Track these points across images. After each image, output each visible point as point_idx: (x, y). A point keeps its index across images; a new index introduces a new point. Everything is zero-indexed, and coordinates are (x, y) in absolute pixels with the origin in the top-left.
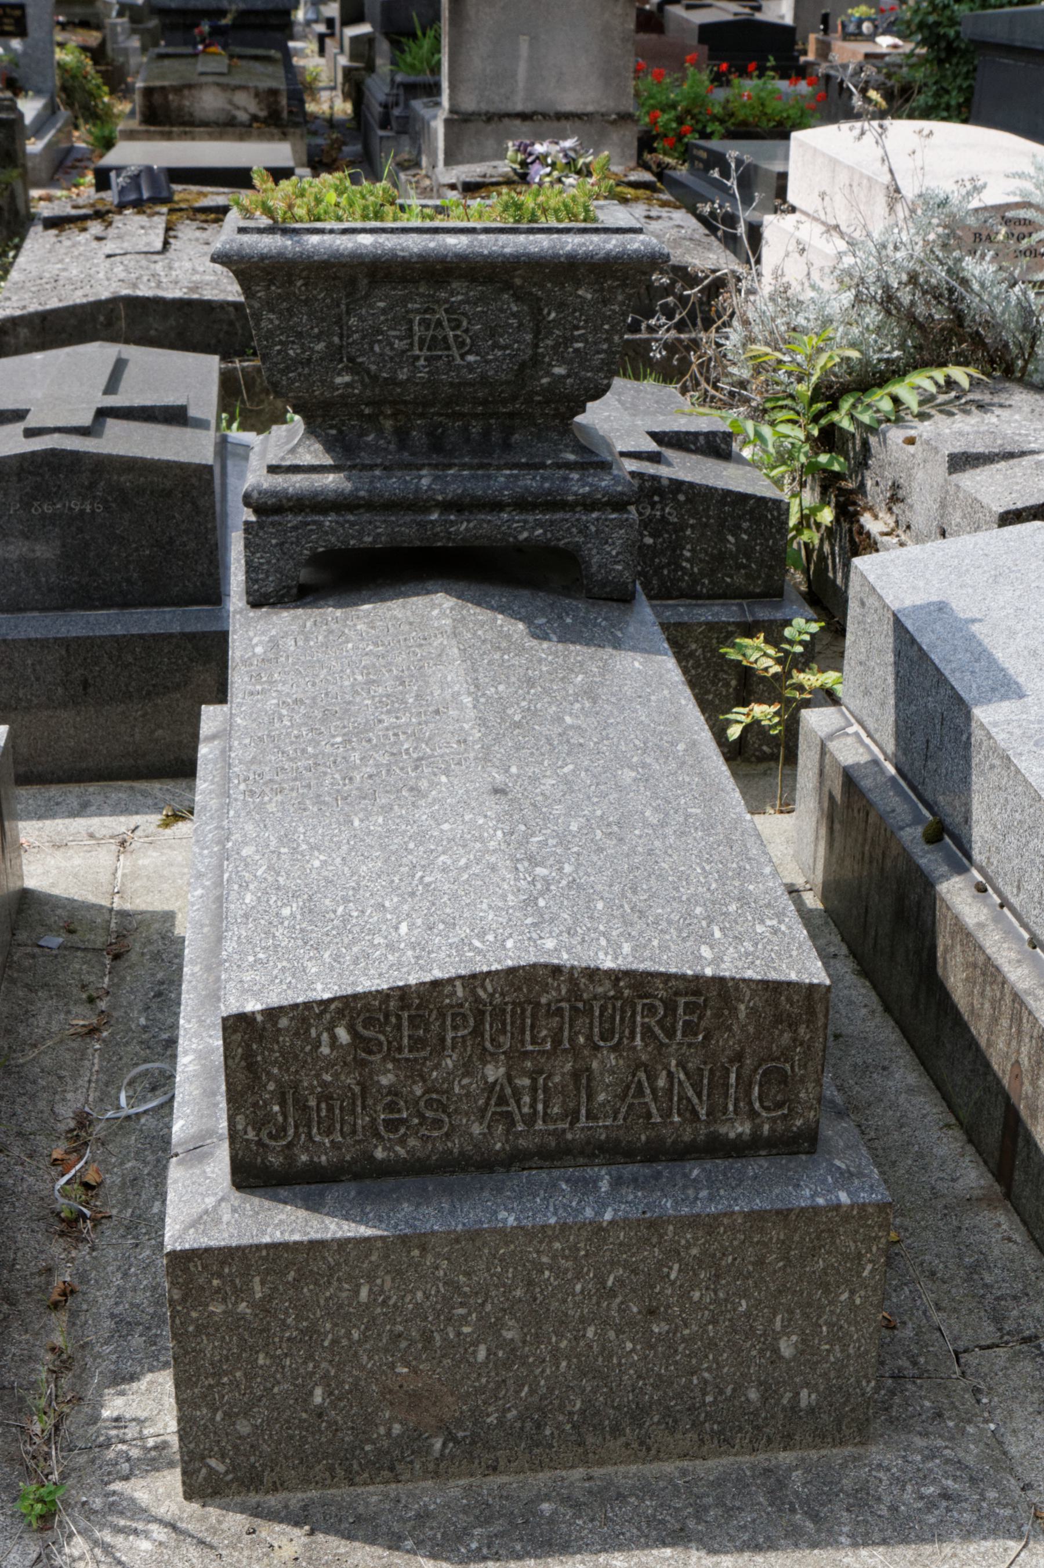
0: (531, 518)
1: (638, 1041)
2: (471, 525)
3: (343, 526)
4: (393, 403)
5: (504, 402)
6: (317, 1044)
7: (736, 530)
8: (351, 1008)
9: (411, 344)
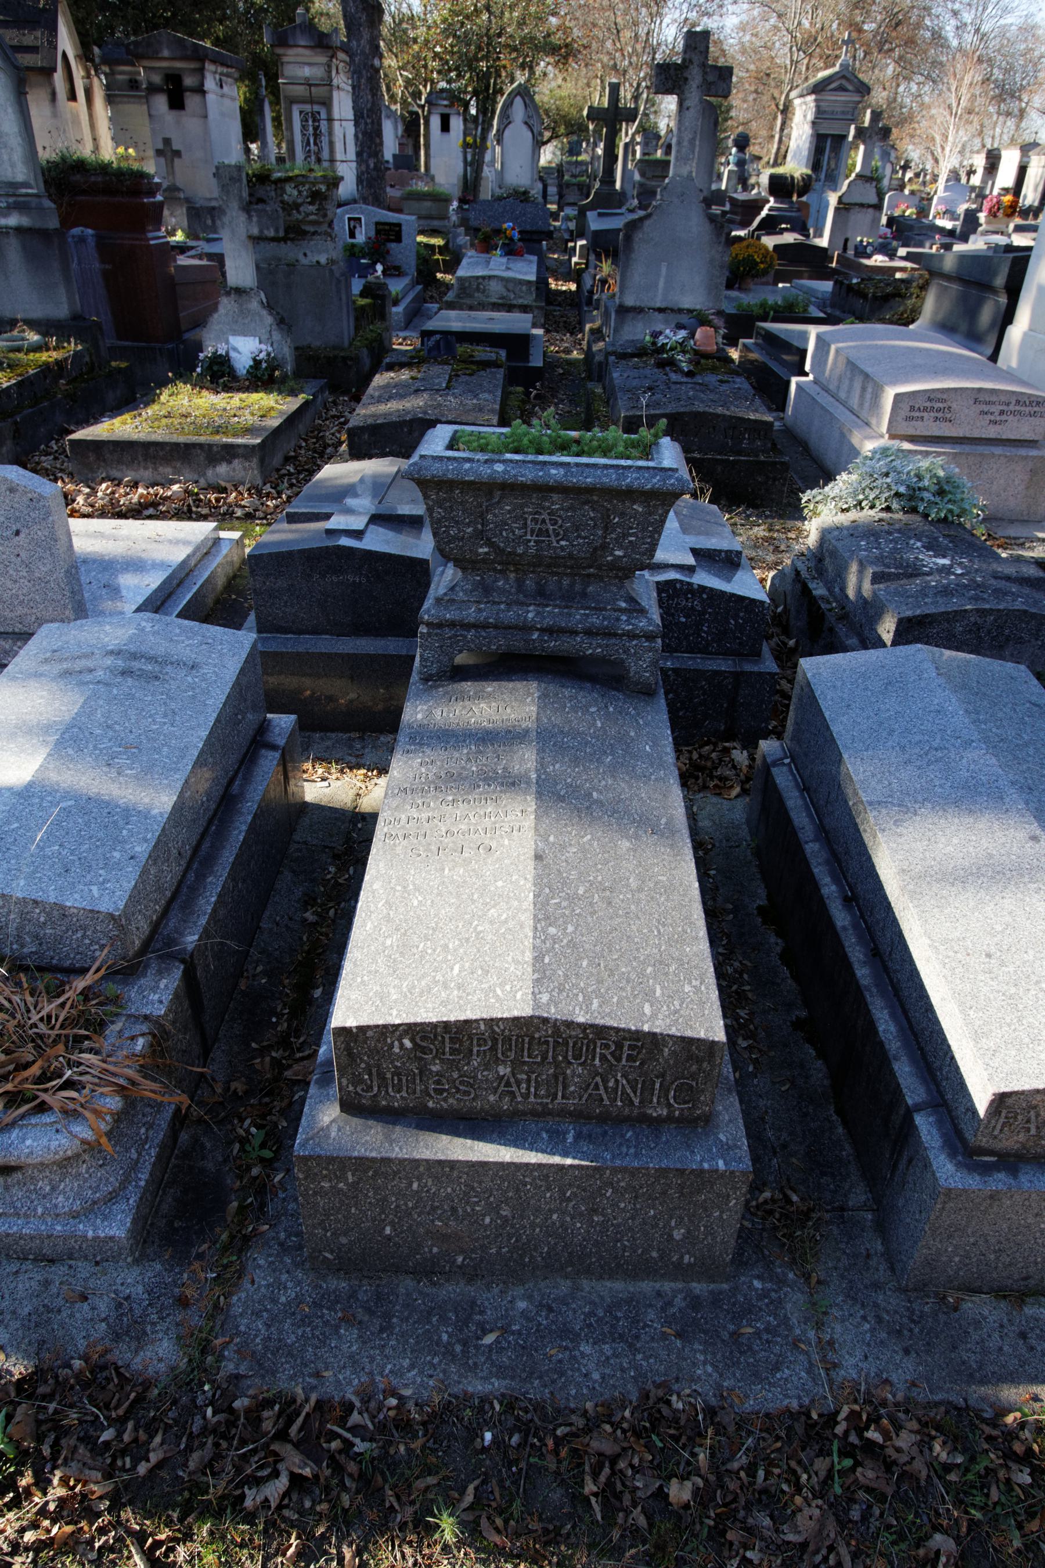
1: (597, 1062)
4: (515, 565)
5: (584, 568)
6: (392, 1046)
7: (736, 617)
8: (412, 1029)
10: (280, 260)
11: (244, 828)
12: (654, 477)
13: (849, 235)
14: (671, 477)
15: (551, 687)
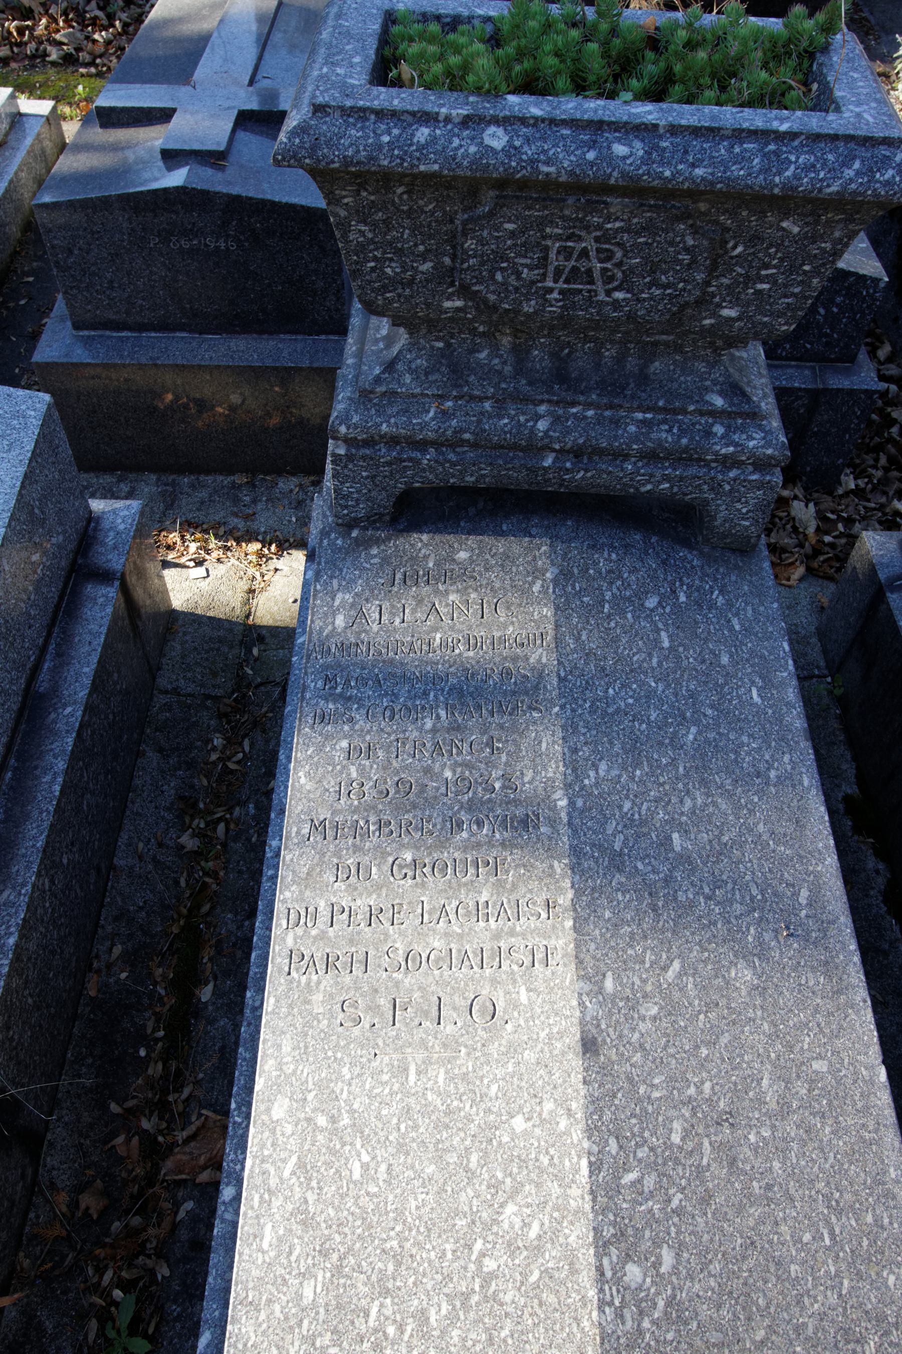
3: (442, 465)
9: (544, 275)
11: (61, 765)
12: (846, 163)
14: (886, 161)
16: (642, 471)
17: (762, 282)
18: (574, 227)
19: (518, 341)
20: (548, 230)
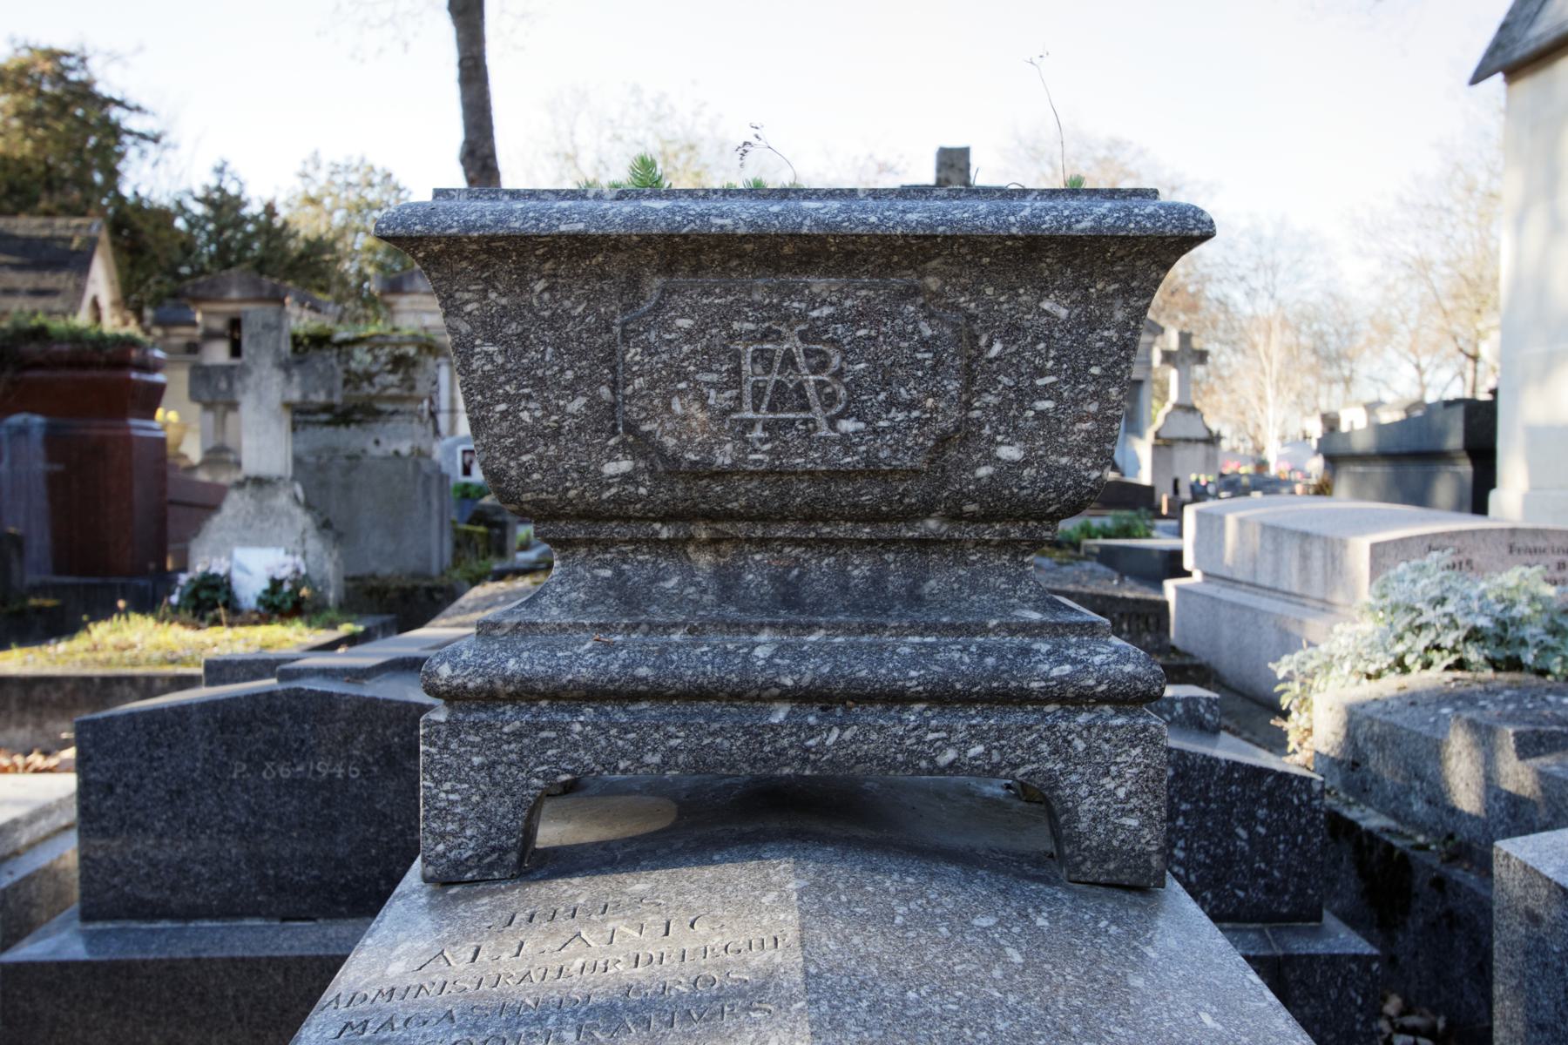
0: (961, 726)
2: (848, 735)
3: (605, 732)
7: (1249, 820)
9: (739, 398)
10: (335, 450)
13: (1177, 474)
15: (838, 870)
16: (934, 722)
17: (1042, 398)
18: (770, 318)
19: (721, 561)
20: (736, 325)
